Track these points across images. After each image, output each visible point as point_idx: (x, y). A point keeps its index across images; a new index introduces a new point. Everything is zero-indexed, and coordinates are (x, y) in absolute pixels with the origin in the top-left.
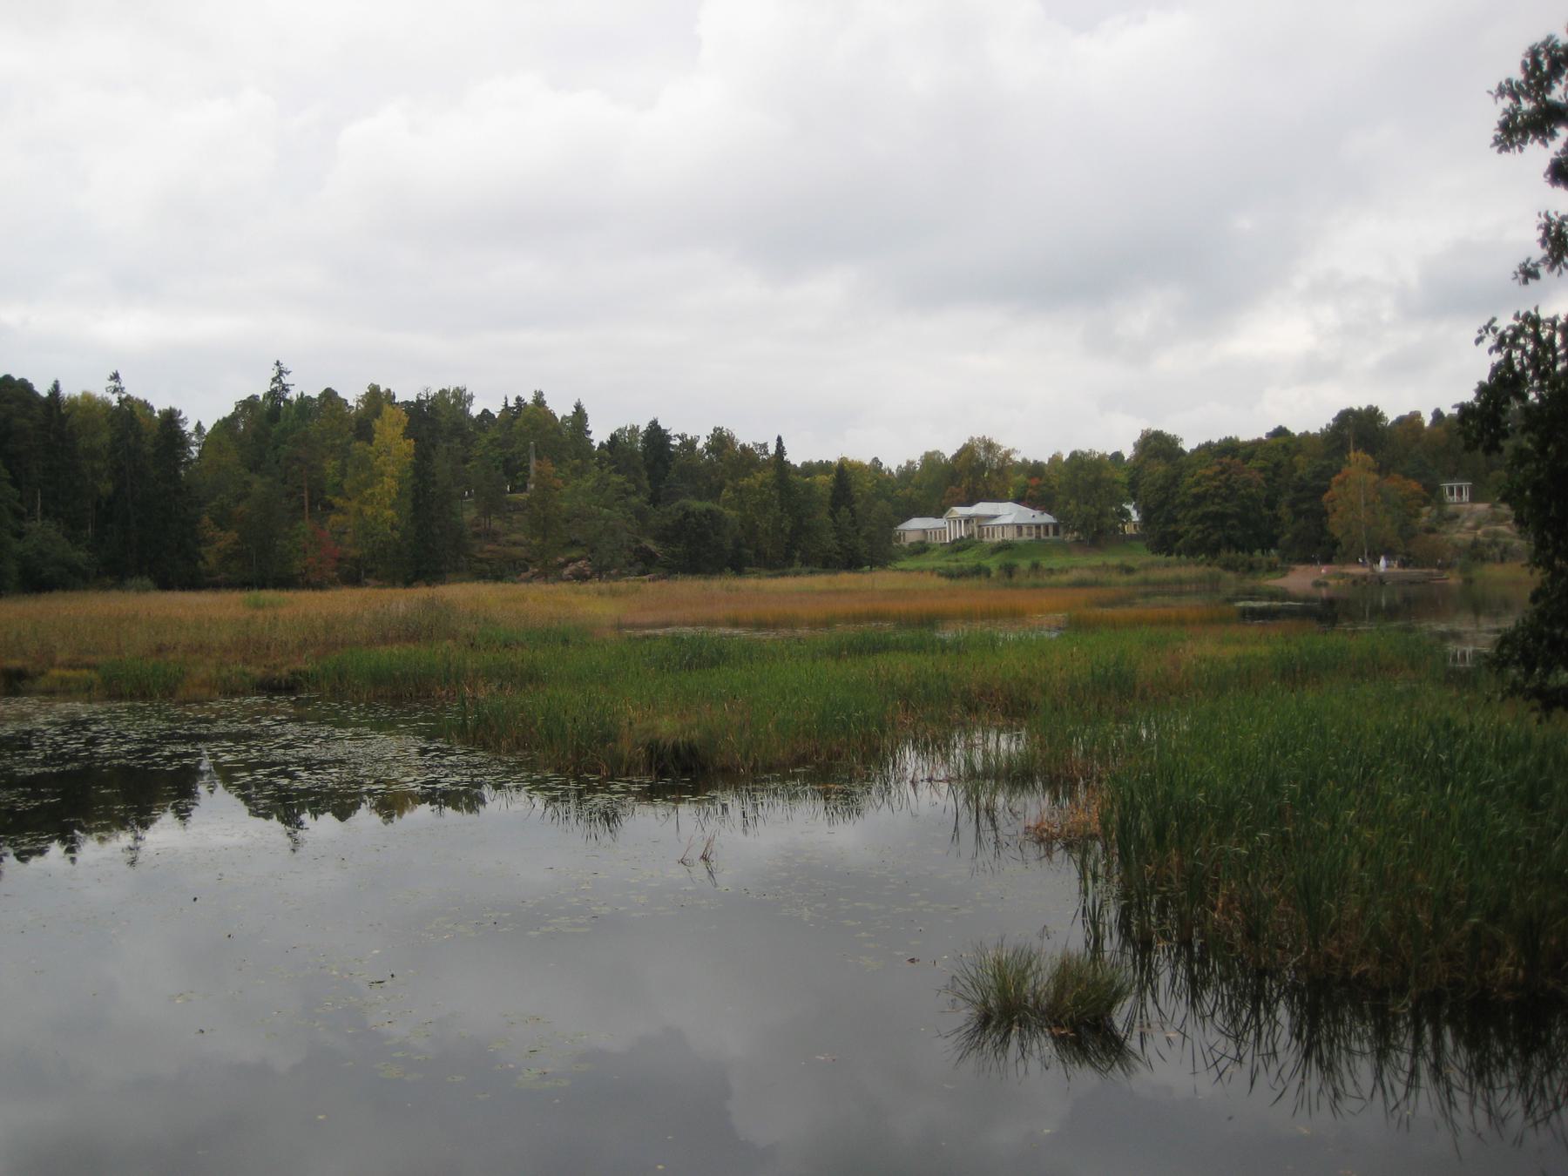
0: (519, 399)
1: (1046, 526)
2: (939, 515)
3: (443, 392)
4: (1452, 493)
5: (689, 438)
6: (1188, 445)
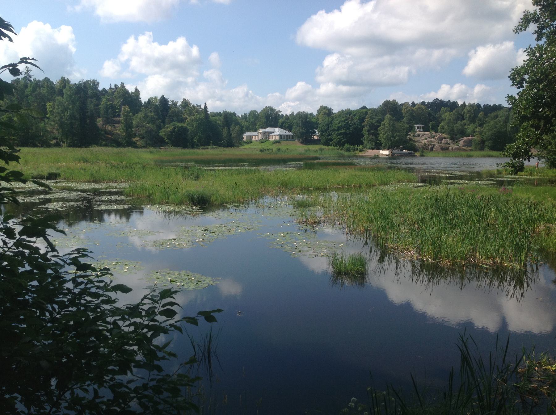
0: (115, 85)
1: (290, 136)
2: (256, 131)
3: (88, 81)
4: (418, 129)
5: (175, 102)
6: (335, 111)
